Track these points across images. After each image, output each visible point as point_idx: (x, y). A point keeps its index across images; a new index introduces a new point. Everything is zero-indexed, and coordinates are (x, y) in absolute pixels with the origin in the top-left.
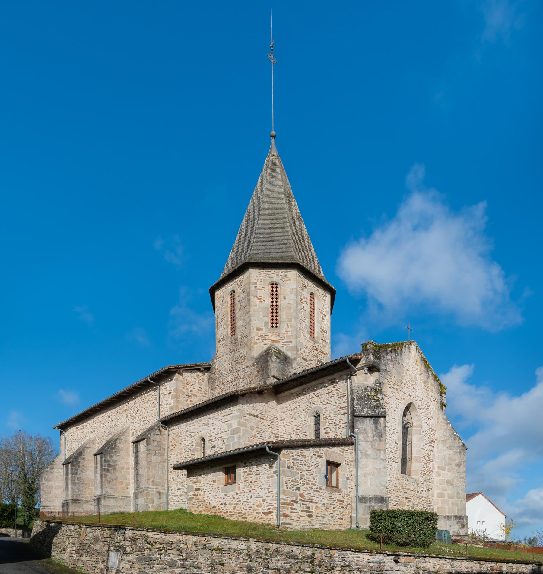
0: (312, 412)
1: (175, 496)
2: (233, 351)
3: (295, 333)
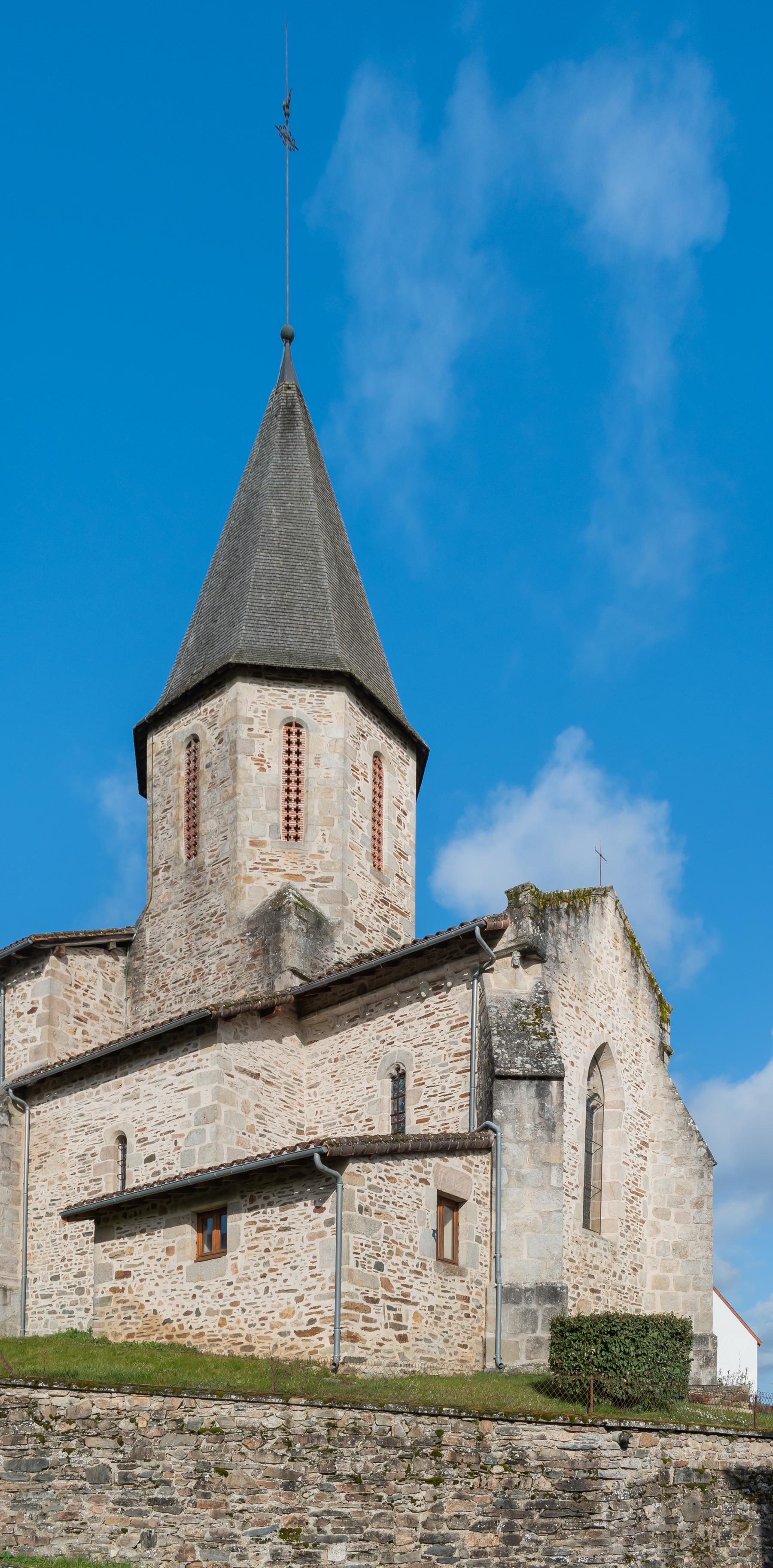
0: (387, 1065)
1: (44, 1297)
2: (191, 899)
3: (339, 857)
